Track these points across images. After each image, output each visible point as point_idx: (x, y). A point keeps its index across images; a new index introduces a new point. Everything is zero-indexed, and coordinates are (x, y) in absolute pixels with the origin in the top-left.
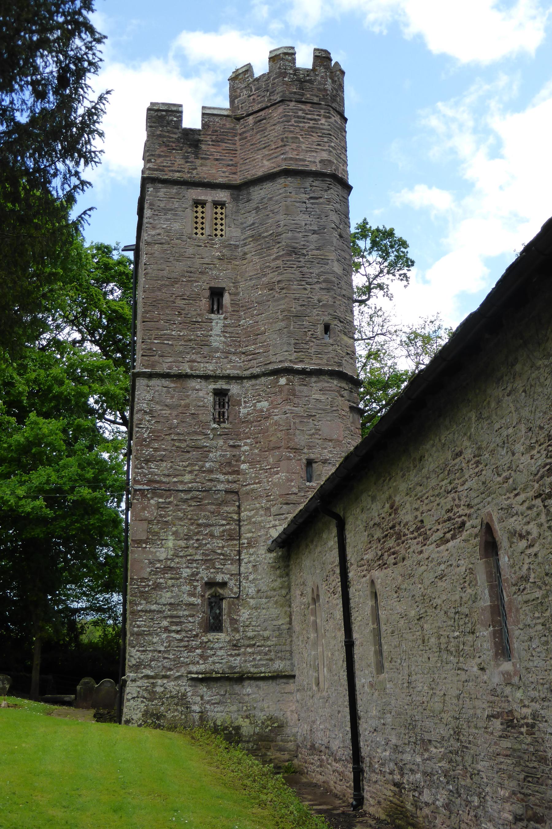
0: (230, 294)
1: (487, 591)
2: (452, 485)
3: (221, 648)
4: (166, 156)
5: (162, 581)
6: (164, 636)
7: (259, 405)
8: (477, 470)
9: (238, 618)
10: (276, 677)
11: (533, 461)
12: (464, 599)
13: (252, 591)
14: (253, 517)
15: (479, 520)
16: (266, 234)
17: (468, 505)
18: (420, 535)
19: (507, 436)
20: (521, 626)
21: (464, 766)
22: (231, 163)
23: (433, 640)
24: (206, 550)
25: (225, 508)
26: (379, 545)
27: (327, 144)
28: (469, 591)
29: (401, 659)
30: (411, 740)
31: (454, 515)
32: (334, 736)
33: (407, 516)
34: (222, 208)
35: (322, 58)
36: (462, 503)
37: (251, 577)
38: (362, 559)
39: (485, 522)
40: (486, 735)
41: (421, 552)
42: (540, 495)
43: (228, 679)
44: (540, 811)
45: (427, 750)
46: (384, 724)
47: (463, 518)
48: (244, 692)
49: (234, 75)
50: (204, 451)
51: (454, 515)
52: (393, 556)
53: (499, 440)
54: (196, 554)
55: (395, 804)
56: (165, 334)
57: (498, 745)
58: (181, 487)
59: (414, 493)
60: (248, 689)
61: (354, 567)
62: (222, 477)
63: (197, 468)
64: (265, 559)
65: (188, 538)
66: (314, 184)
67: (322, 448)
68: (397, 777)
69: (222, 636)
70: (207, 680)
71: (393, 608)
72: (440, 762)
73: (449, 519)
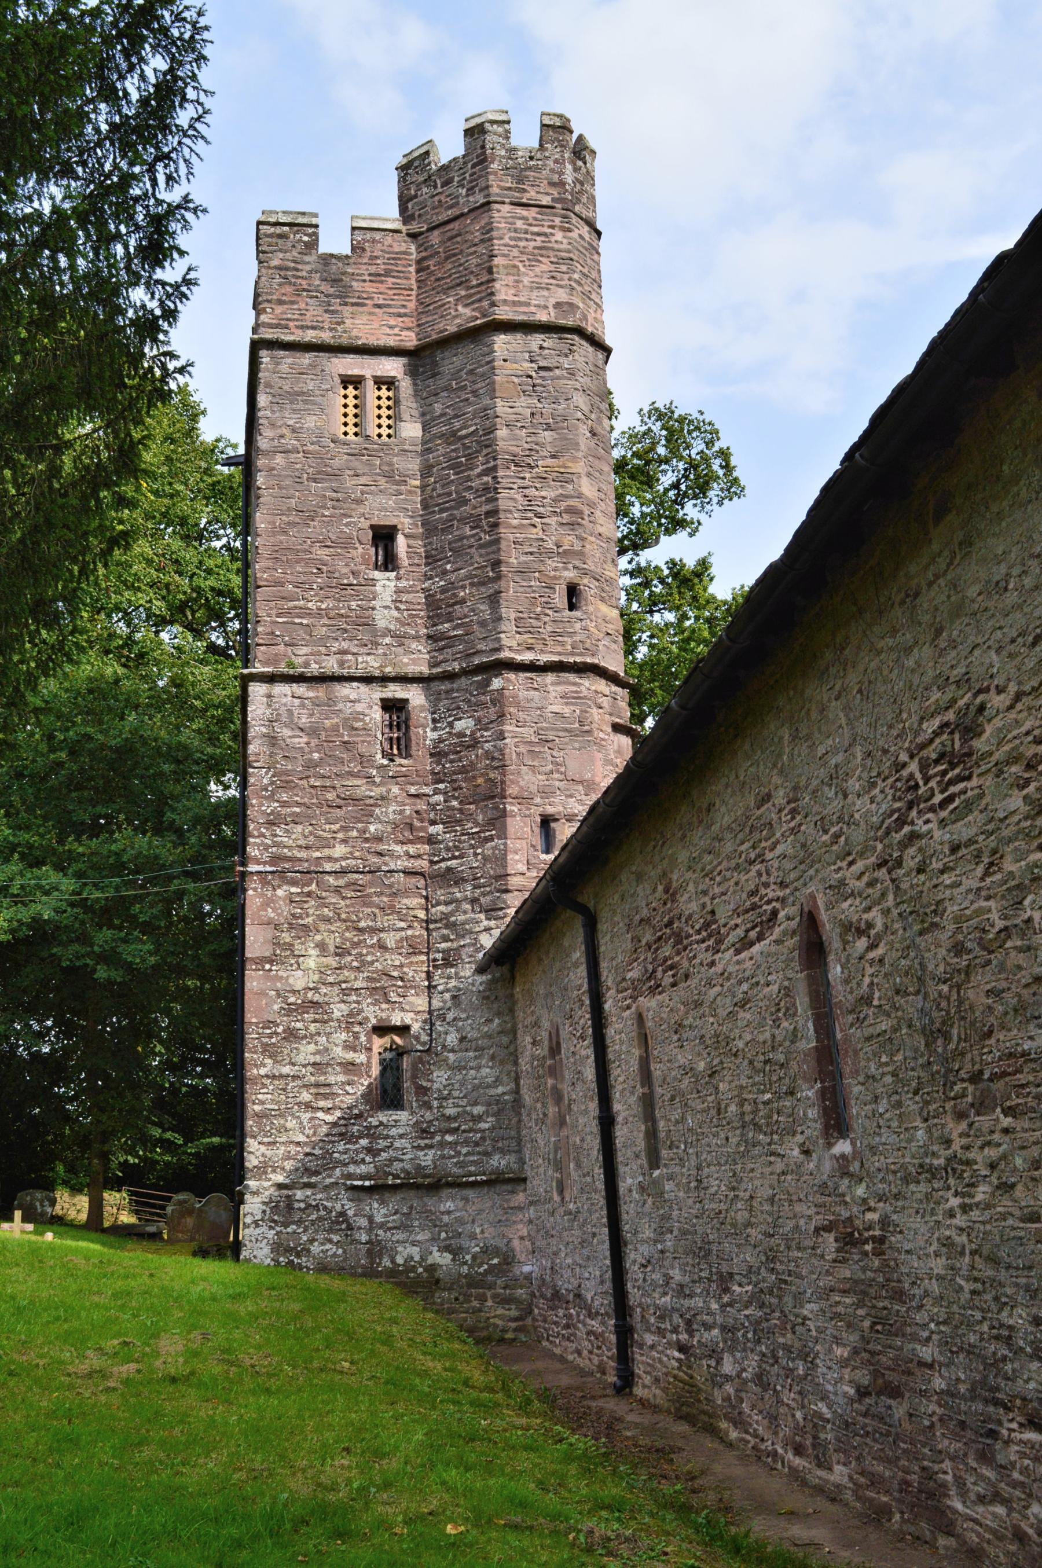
0: (406, 536)
1: (810, 1025)
2: (757, 851)
3: (401, 1136)
4: (292, 303)
5: (299, 1025)
6: (306, 1116)
7: (459, 726)
8: (792, 824)
9: (429, 1085)
10: (497, 1181)
11: (874, 805)
12: (778, 1039)
13: (452, 1039)
14: (452, 914)
15: (797, 907)
16: (464, 432)
17: (781, 883)
18: (710, 936)
19: (836, 766)
20: (861, 1079)
21: (782, 1312)
22: (402, 311)
23: (733, 1108)
24: (373, 972)
25: (405, 901)
26: (649, 955)
27: (566, 276)
28: (785, 1024)
29: (686, 1143)
30: (703, 1274)
31: (761, 899)
32: (587, 1275)
33: (689, 904)
34: (389, 389)
35: (556, 129)
36: (772, 880)
37: (450, 1016)
38: (624, 979)
39: (806, 909)
40: (814, 1260)
41: (712, 964)
42: (885, 863)
43: (417, 1187)
44: (892, 1377)
45: (726, 1290)
46: (662, 1252)
47: (774, 904)
48: (442, 1209)
49: (405, 161)
50: (365, 809)
51: (761, 899)
52: (670, 973)
53: (822, 773)
54: (356, 979)
55: (681, 1381)
56: (296, 607)
57: (831, 1274)
58: (328, 867)
59: (700, 866)
60: (448, 1204)
61: (612, 992)
62: (399, 849)
63: (355, 833)
64: (473, 985)
65: (341, 952)
66: (545, 345)
67: (567, 796)
68: (684, 1337)
69: (403, 1116)
70: (379, 1189)
71: (674, 1059)
72: (747, 1308)
73: (754, 907)
